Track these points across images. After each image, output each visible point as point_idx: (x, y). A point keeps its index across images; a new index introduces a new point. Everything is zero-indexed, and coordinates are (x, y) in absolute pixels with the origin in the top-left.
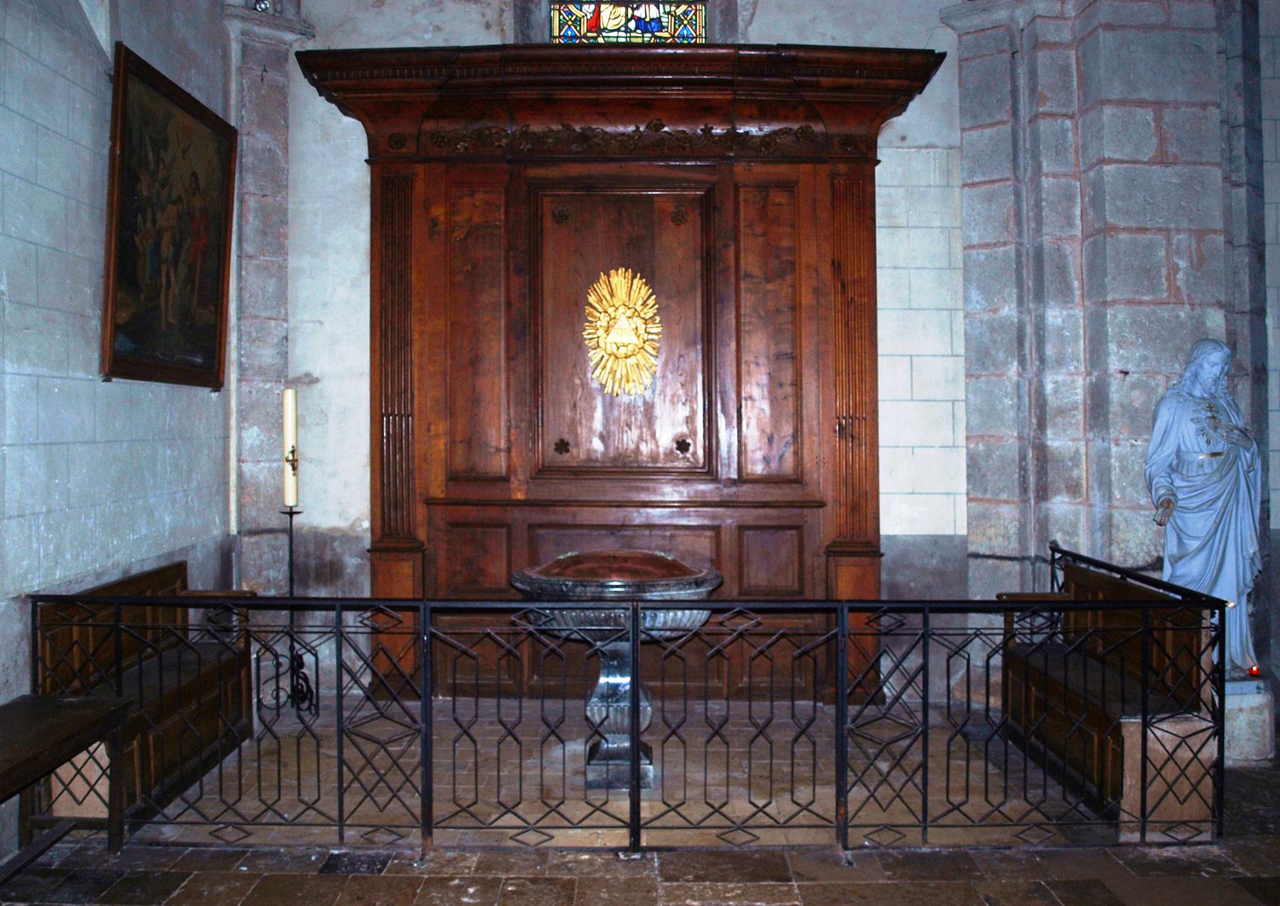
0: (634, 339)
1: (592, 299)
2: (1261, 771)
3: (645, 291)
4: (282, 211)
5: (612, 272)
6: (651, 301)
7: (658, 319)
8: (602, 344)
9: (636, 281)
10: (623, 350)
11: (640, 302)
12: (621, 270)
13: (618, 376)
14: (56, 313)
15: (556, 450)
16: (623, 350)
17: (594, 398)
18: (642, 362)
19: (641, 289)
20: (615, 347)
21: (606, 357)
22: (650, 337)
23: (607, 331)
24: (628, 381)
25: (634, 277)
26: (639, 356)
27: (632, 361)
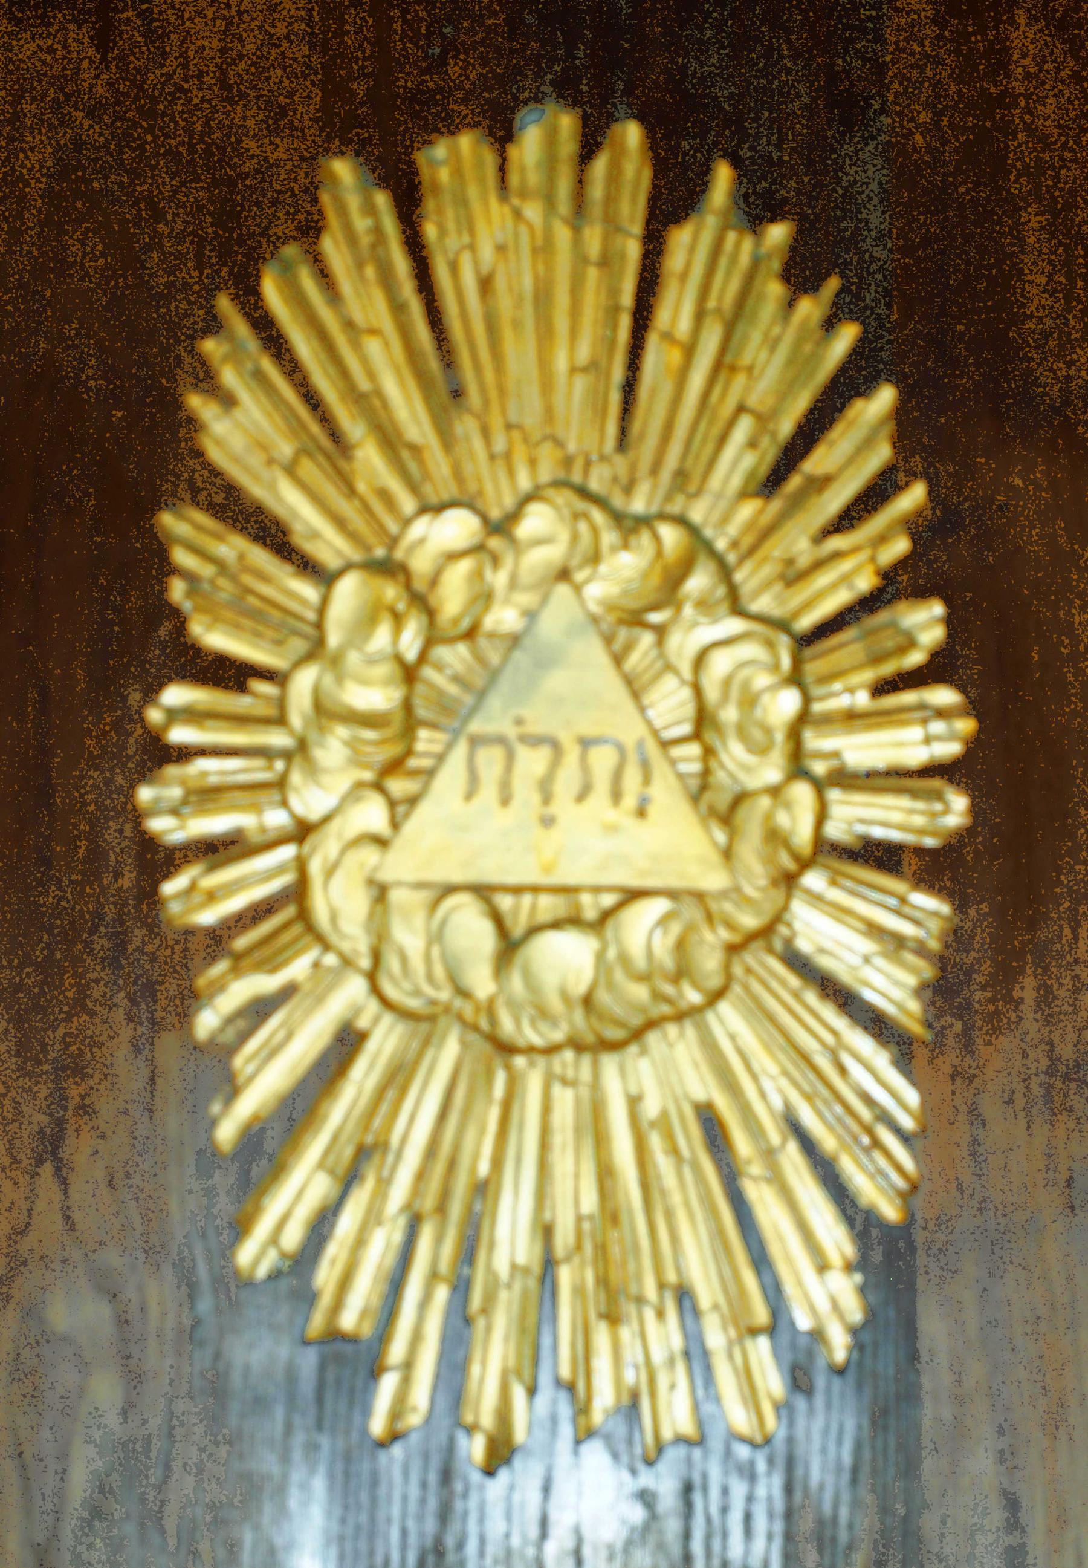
0: (674, 844)
1: (240, 428)
2: (944, 650)
3: (794, 344)
4: (856, 860)
5: (453, 158)
6: (863, 438)
7: (925, 623)
8: (340, 902)
9: (685, 244)
10: (565, 959)
11: (738, 460)
12: (544, 135)
13: (511, 1241)
14: (537, 1040)
15: (1004, 1435)
16: (565, 959)
17: (253, 1493)
18: (772, 1088)
19: (747, 325)
20: (471, 931)
21: (384, 1041)
22: (856, 816)
23: (395, 770)
24: (612, 1304)
25: (672, 202)
26: (729, 1020)
27: (666, 1074)
